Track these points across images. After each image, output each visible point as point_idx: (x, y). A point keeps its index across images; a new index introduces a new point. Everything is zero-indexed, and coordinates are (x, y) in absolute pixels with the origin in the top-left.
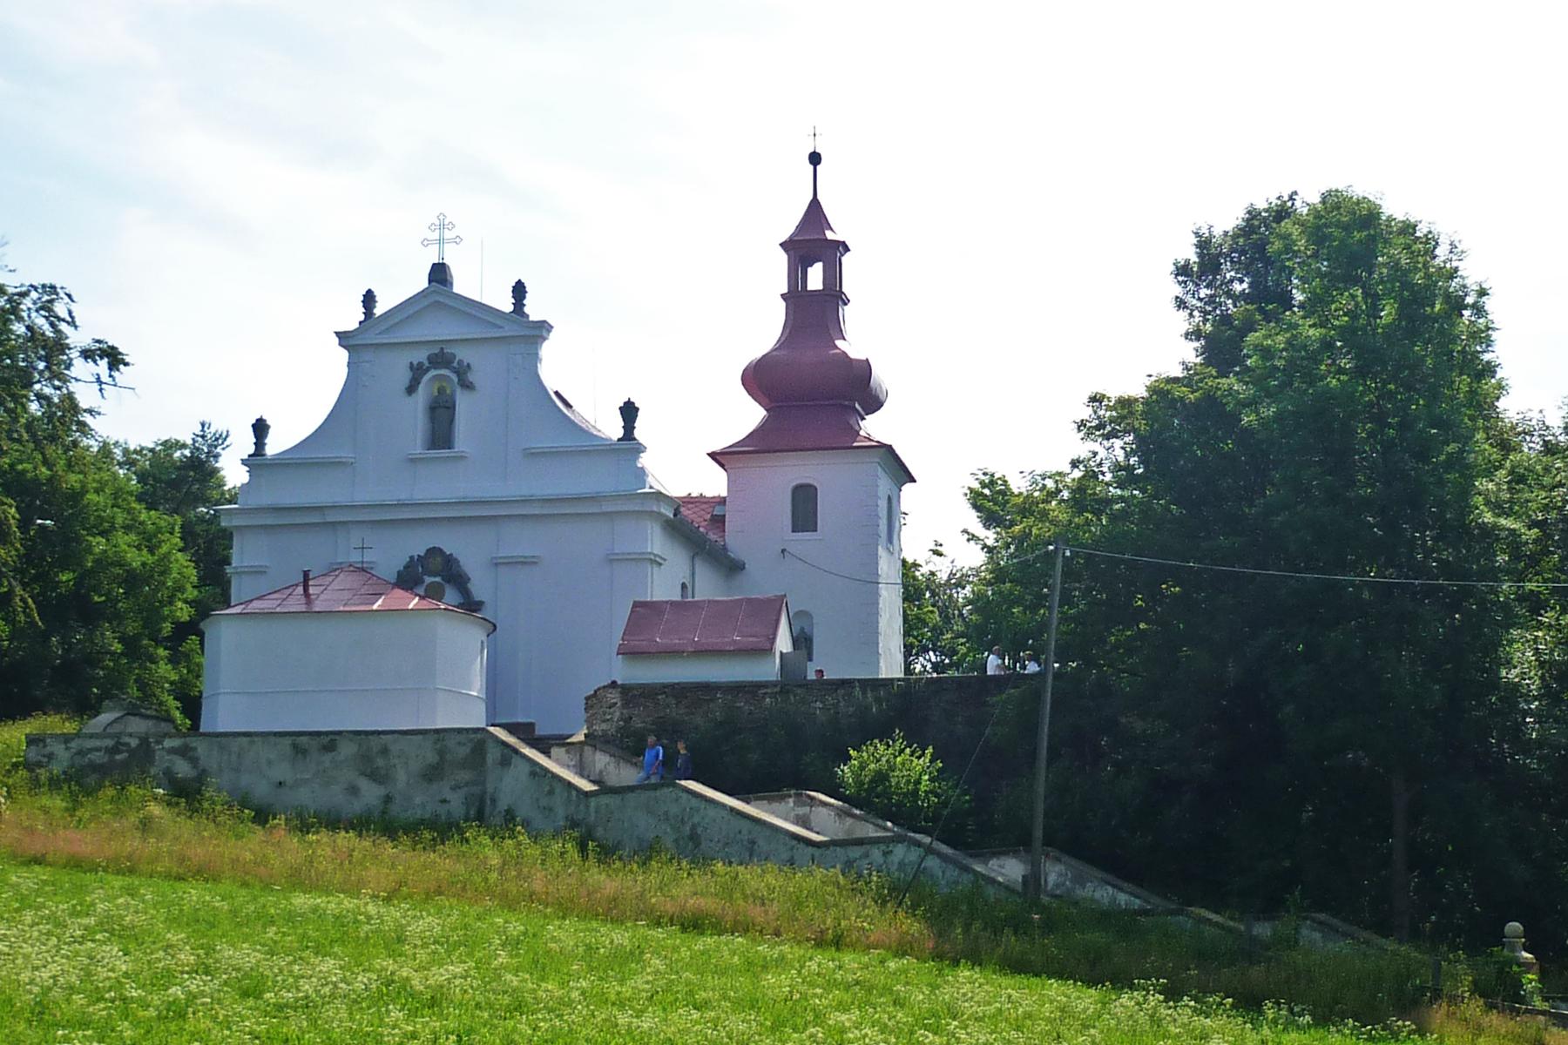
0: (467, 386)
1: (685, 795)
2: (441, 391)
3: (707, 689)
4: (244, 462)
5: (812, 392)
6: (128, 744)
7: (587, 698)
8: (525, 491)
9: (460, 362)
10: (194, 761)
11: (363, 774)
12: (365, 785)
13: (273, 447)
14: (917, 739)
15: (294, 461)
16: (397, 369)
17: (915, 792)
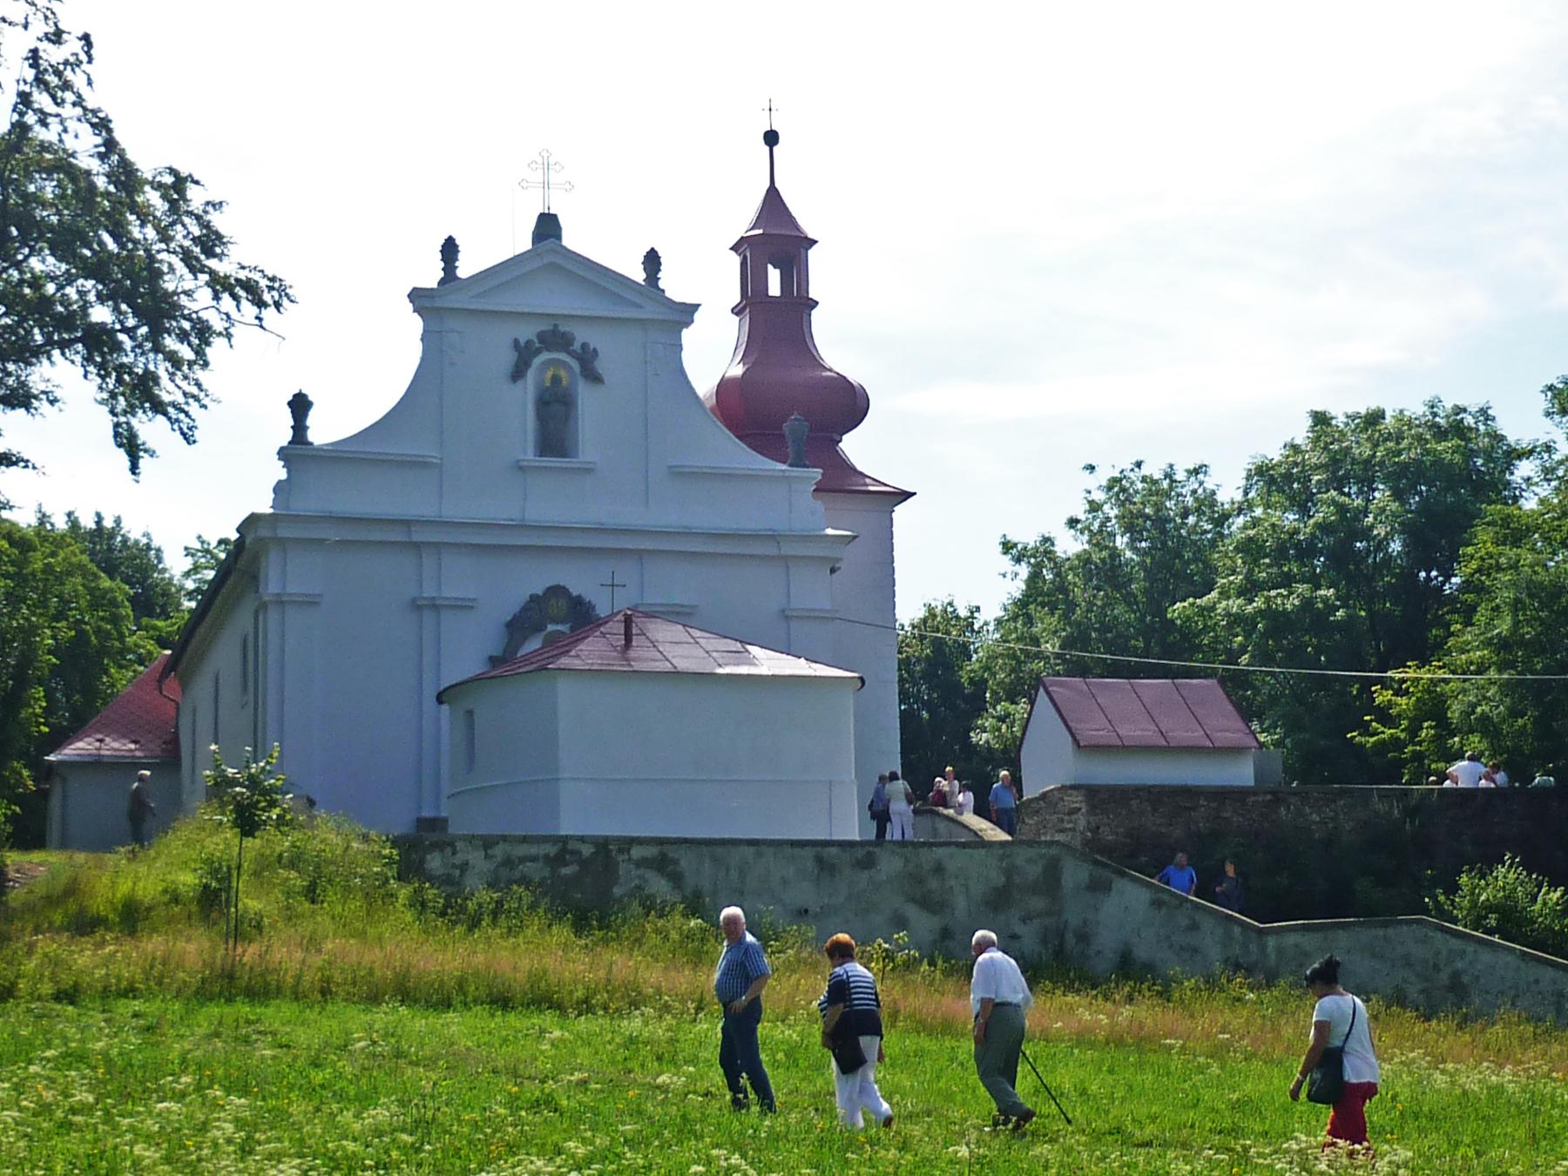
0: (593, 377)
2: (556, 380)
3: (1187, 794)
6: (579, 853)
9: (584, 346)
11: (913, 900)
13: (322, 431)
15: (349, 456)
16: (496, 348)
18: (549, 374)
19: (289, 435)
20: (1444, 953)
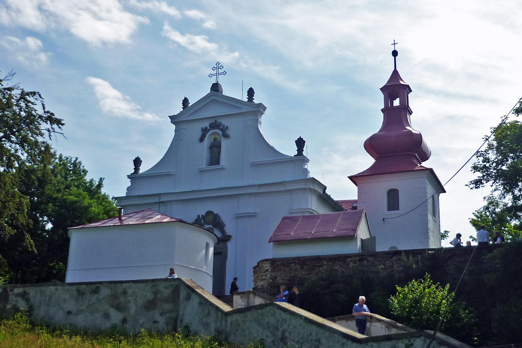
0: (226, 136)
1: (278, 311)
2: (215, 139)
4: (129, 177)
5: (397, 150)
7: (254, 268)
8: (251, 183)
10: (27, 300)
11: (112, 306)
12: (112, 312)
14: (440, 280)
16: (196, 130)
17: (438, 312)
18: (213, 136)
19: (133, 171)
20: (280, 320)
